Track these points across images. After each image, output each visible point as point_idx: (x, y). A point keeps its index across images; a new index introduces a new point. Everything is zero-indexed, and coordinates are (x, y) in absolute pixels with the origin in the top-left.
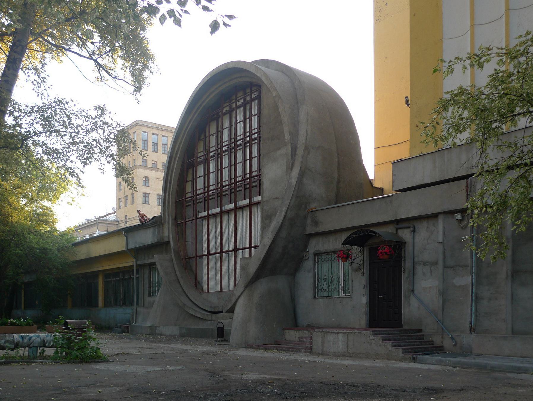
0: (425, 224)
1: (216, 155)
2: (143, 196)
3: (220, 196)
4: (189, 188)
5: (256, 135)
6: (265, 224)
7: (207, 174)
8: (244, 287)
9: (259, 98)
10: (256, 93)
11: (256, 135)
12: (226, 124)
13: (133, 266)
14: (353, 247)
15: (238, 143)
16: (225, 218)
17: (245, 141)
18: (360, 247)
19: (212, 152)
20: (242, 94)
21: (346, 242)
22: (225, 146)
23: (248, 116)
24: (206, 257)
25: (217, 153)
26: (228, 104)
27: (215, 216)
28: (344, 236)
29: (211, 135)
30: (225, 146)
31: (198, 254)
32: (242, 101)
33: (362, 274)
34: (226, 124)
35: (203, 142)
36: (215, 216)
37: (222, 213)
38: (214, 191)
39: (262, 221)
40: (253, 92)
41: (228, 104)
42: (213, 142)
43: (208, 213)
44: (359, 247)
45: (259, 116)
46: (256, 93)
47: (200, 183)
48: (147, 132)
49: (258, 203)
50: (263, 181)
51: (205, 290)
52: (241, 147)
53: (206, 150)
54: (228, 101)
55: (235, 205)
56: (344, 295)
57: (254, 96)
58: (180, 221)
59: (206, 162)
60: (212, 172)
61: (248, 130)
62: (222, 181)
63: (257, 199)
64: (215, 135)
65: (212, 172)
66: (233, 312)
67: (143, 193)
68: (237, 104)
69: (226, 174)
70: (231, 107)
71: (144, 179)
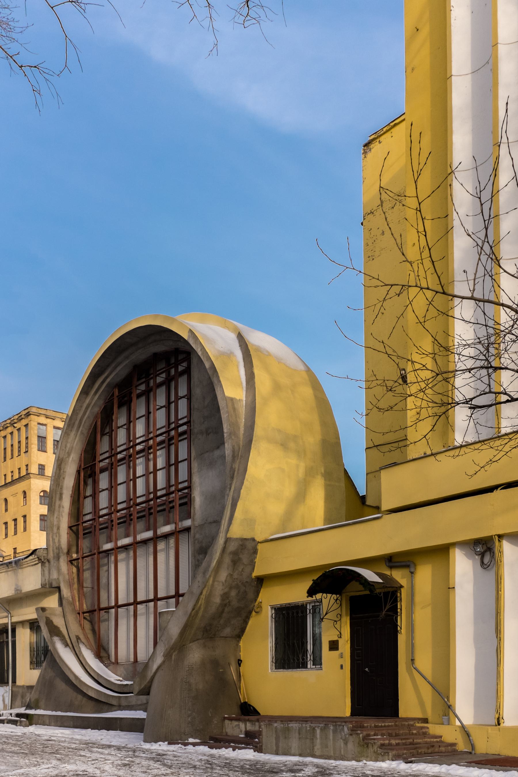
0: (62, 610)
1: (127, 458)
2: (41, 520)
3: (109, 526)
4: (88, 506)
5: (185, 428)
6: (198, 560)
7: (112, 488)
8: (163, 656)
9: (188, 371)
10: (185, 364)
11: (185, 428)
12: (141, 411)
13: (8, 623)
14: (325, 595)
15: (181, 430)
16: (161, 546)
17: (169, 435)
18: (336, 594)
19: (120, 452)
20: (164, 366)
21: (311, 592)
22: (139, 444)
23: (173, 398)
24: (113, 610)
25: (128, 454)
26: (144, 380)
27: (127, 549)
28: (307, 584)
29: (119, 428)
30: (139, 444)
31: (103, 605)
32: (164, 375)
33: (339, 636)
34: (141, 411)
35: (108, 437)
36: (127, 549)
37: (155, 539)
38: (144, 505)
39: (194, 556)
40: (158, 373)
41: (144, 380)
42: (121, 437)
43: (155, 532)
44: (334, 595)
45: (189, 398)
46: (185, 364)
47: (103, 499)
48: (45, 425)
49: (188, 530)
50: (194, 497)
51: (113, 659)
52: (185, 436)
53: (112, 449)
54: (144, 376)
55: (155, 532)
56: (314, 667)
57: (180, 368)
58: (75, 556)
59: (111, 469)
60: (160, 469)
61: (173, 419)
62: (156, 490)
63: (188, 523)
64: (125, 427)
65: (160, 469)
66: (148, 694)
67: (41, 515)
68: (156, 382)
69: (121, 494)
70: (148, 385)
71: (42, 494)
